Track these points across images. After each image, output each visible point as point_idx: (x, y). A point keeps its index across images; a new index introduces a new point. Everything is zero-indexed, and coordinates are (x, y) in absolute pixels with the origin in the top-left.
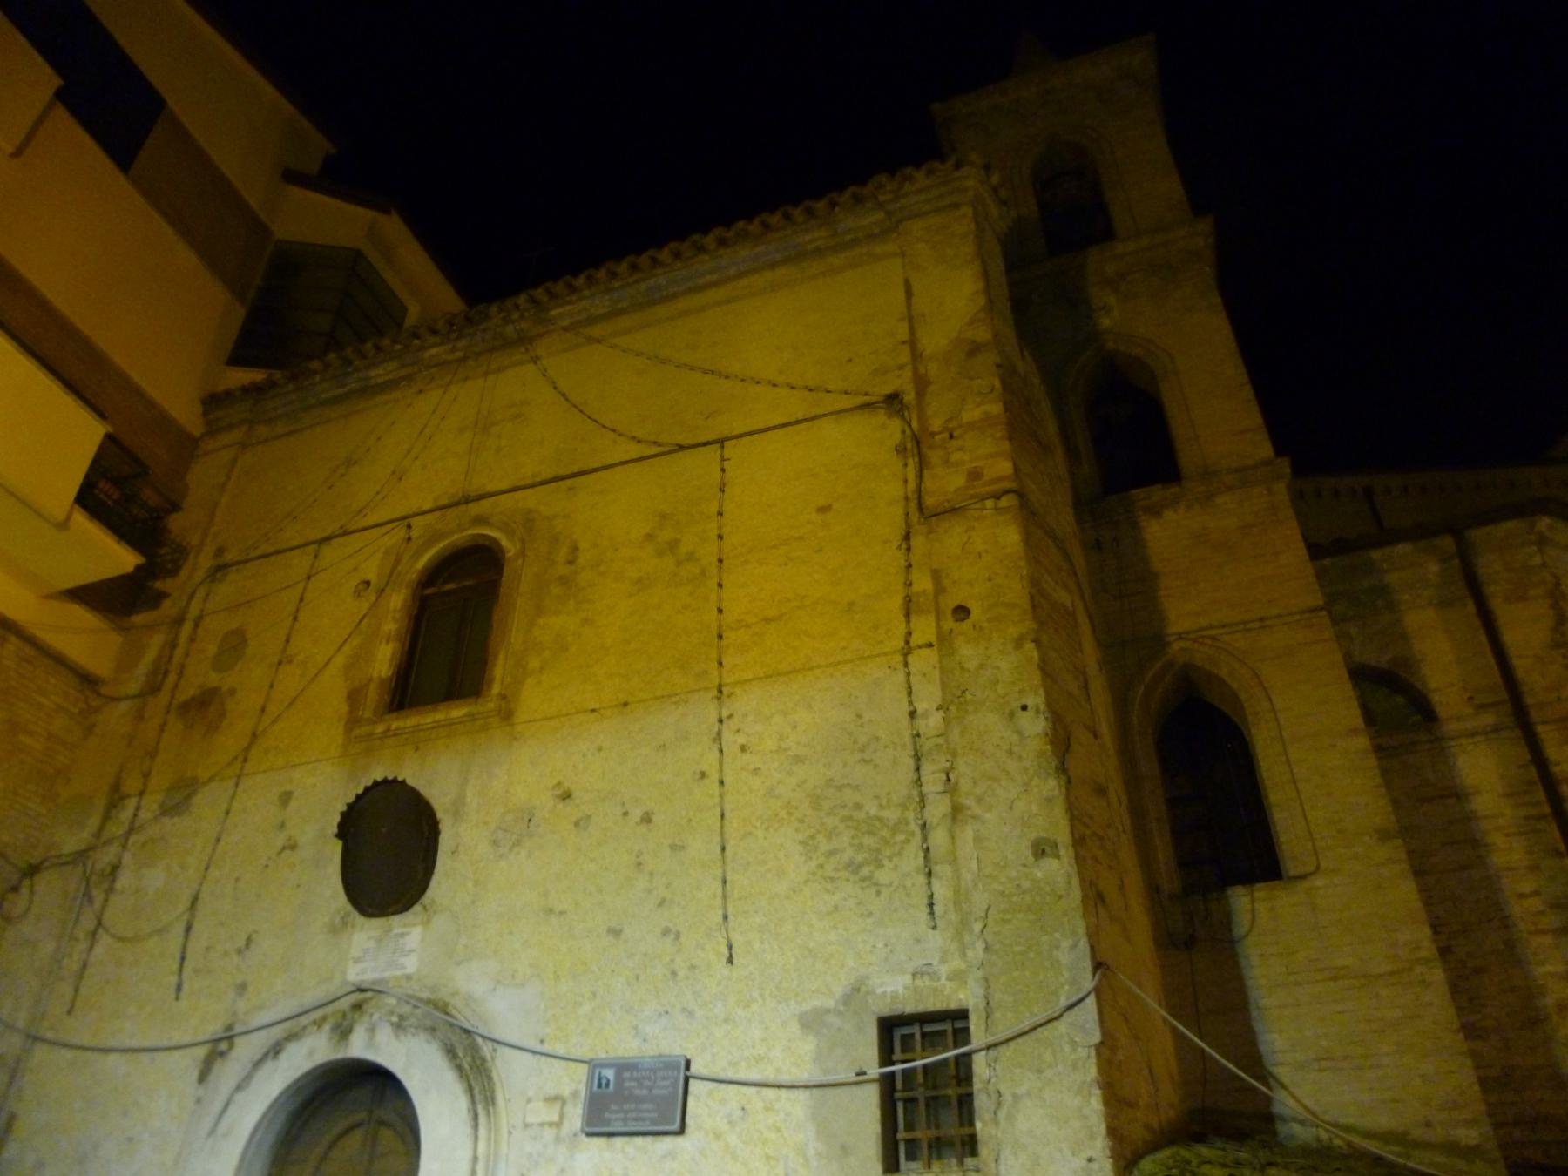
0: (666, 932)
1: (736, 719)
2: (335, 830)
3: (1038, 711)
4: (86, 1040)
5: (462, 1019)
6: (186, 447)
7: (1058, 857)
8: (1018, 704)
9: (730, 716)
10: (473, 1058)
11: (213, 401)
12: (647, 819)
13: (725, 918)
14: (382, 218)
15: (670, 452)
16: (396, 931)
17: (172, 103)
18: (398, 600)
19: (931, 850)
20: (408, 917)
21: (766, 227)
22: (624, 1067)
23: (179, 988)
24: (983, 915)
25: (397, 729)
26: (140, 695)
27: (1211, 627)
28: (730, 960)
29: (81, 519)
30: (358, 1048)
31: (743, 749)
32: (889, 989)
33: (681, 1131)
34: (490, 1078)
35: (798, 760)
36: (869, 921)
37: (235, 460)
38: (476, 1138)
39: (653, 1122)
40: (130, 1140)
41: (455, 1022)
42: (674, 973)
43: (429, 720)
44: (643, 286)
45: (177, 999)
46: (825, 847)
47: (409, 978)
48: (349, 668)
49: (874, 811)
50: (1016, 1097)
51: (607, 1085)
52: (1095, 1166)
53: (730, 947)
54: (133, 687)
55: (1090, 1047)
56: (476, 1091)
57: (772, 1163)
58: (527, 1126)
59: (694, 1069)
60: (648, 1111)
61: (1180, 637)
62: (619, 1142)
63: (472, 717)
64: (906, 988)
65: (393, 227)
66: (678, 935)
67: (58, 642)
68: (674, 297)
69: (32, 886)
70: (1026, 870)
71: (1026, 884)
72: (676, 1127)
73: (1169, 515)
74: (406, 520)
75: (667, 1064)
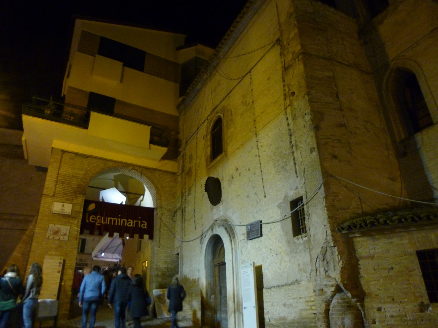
0: (255, 194)
1: (260, 140)
2: (205, 190)
3: (309, 114)
4: (188, 240)
5: (229, 222)
6: (176, 119)
7: (315, 151)
8: (305, 114)
9: (259, 140)
10: (230, 229)
11: (178, 107)
12: (249, 170)
13: (264, 187)
14: (197, 47)
15: (242, 79)
16: (219, 207)
17: (147, 50)
18: (209, 137)
19: (295, 158)
20: (220, 204)
21: (248, 8)
22: (251, 225)
23: (196, 228)
24: (303, 171)
25: (212, 165)
26: (181, 173)
27: (402, 52)
28: (265, 196)
29: (152, 146)
30: (215, 232)
31: (262, 146)
32: (291, 194)
33: (261, 235)
34: (234, 232)
35: (271, 145)
36: (287, 179)
37: (184, 118)
38: (232, 245)
39: (257, 235)
40: (195, 256)
41: (228, 223)
42: (257, 202)
43: (216, 161)
44: (232, 39)
45: (196, 229)
46: (277, 165)
47: (222, 216)
48: (205, 155)
49: (284, 152)
50: (311, 213)
51: (249, 229)
52: (326, 226)
53: (265, 194)
54: (180, 172)
55: (323, 198)
56: (231, 236)
57: (276, 239)
58: (241, 240)
59: (263, 222)
60: (255, 233)
61: (393, 60)
62: (253, 240)
63: (222, 158)
64: (294, 193)
65: (200, 47)
66: (257, 193)
67: (164, 168)
68: (238, 37)
69: (176, 215)
70: (310, 157)
71: (310, 160)
72: (259, 235)
73: (386, 21)
74: (207, 119)
75: (257, 222)
